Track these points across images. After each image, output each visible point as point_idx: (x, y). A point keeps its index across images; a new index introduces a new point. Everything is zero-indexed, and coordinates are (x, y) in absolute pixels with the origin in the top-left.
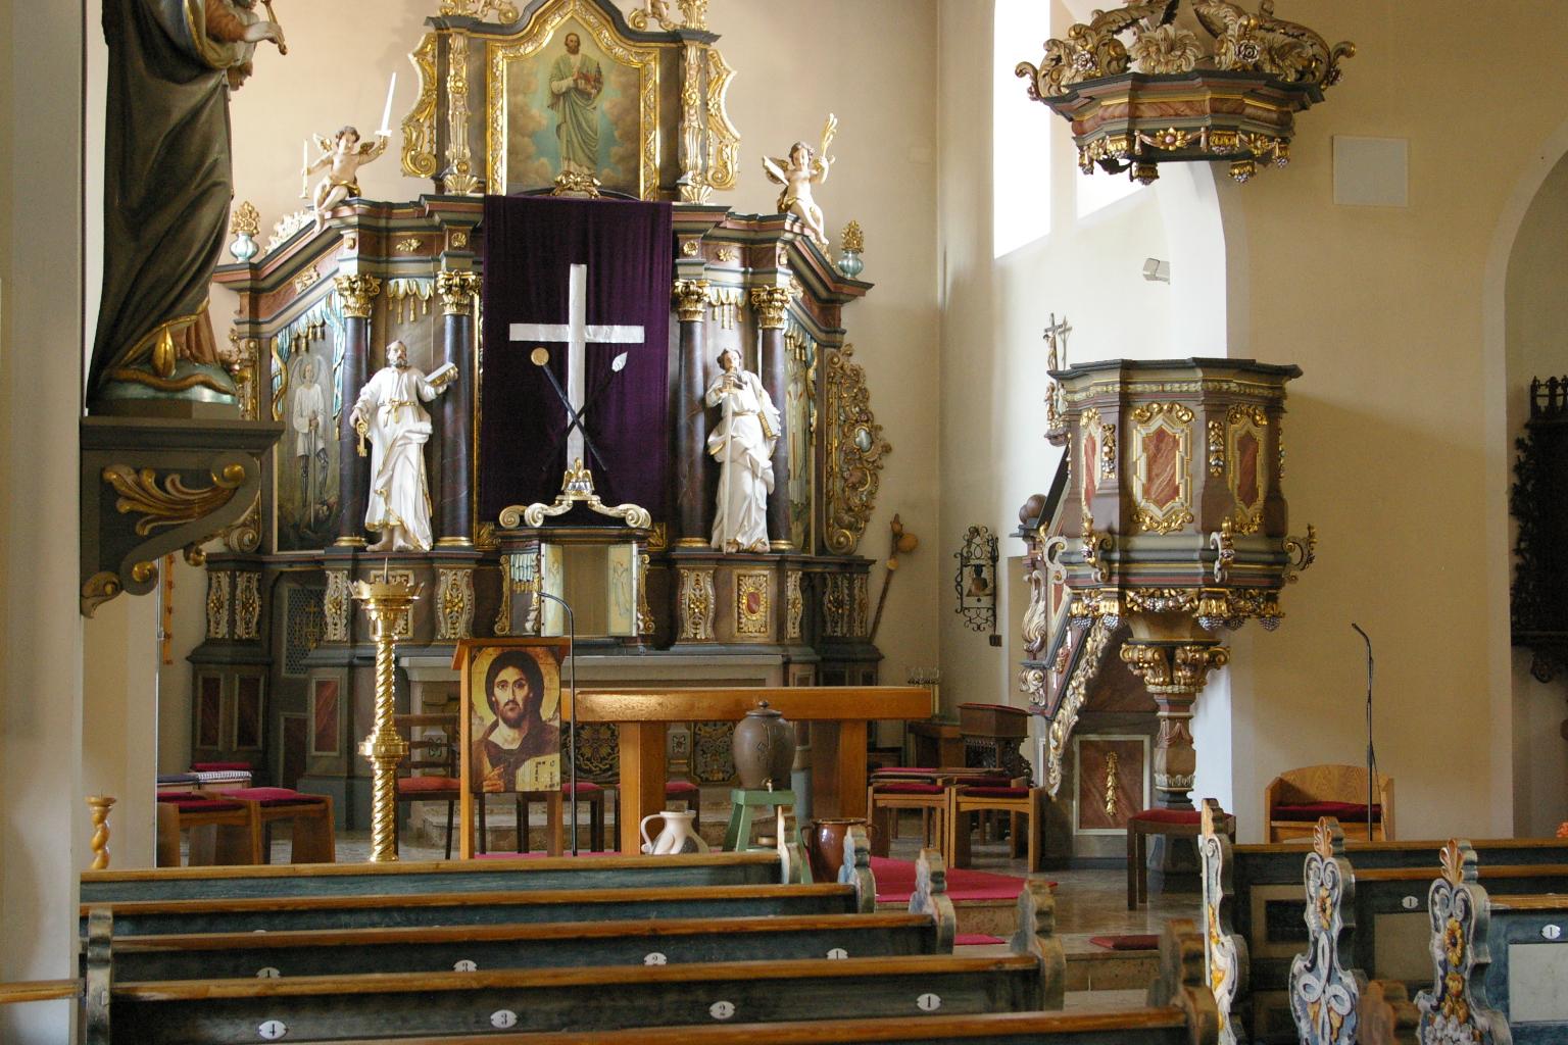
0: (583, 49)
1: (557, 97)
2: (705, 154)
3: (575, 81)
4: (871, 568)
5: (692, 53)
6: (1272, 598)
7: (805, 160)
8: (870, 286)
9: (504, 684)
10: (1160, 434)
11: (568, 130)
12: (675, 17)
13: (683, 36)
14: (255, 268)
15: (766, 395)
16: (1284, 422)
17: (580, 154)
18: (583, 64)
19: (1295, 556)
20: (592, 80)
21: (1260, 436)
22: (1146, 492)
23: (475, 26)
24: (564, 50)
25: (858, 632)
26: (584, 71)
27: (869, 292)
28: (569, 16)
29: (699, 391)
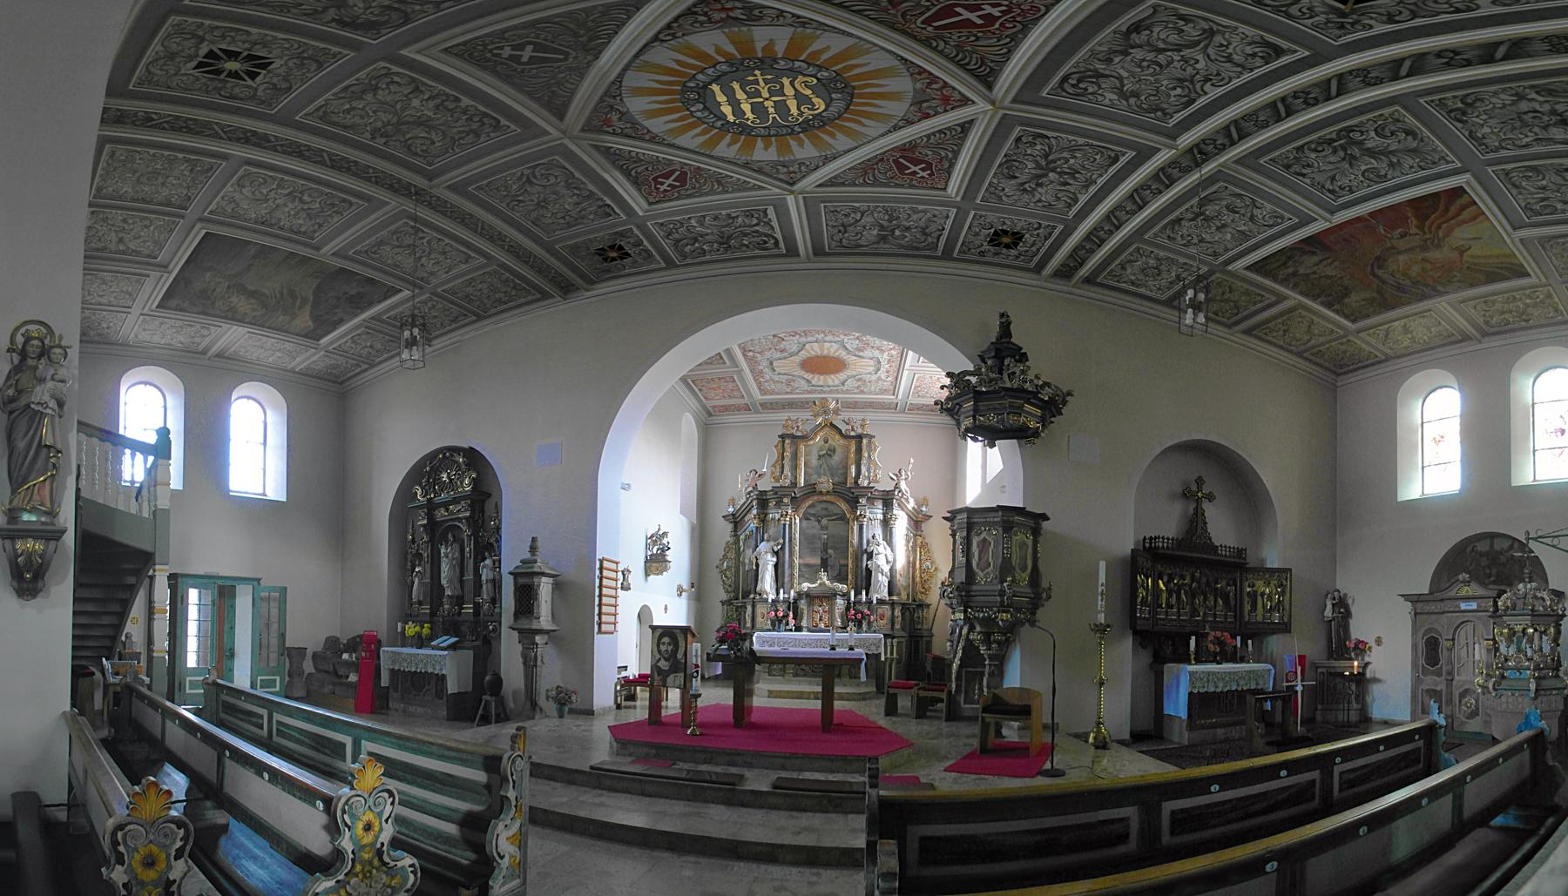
2: (869, 471)
5: (865, 441)
6: (1034, 614)
7: (903, 473)
9: (664, 643)
10: (985, 539)
12: (860, 431)
14: (733, 515)
15: (888, 549)
16: (1041, 539)
19: (1044, 595)
20: (832, 451)
21: (1030, 543)
22: (978, 565)
23: (793, 437)
25: (925, 627)
29: (865, 547)
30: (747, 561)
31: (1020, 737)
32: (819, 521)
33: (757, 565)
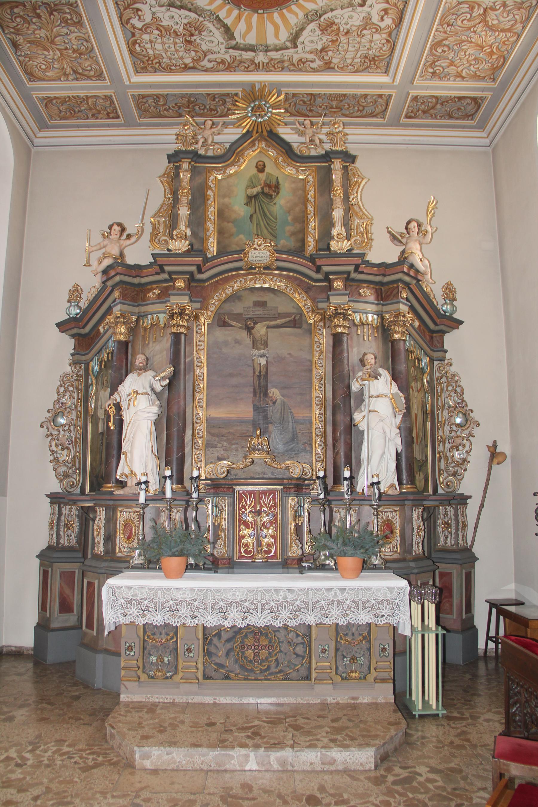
0: (267, 170)
1: (250, 199)
3: (262, 188)
4: (469, 501)
5: (337, 165)
8: (461, 322)
11: (257, 217)
13: (331, 156)
17: (265, 231)
18: (267, 178)
23: (195, 156)
24: (255, 171)
26: (268, 182)
27: (461, 327)
28: (258, 150)
30: (101, 414)
31: (508, 766)
32: (249, 329)
33: (120, 423)
